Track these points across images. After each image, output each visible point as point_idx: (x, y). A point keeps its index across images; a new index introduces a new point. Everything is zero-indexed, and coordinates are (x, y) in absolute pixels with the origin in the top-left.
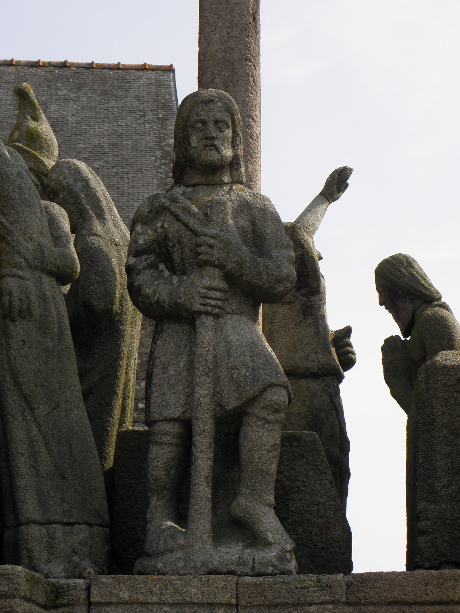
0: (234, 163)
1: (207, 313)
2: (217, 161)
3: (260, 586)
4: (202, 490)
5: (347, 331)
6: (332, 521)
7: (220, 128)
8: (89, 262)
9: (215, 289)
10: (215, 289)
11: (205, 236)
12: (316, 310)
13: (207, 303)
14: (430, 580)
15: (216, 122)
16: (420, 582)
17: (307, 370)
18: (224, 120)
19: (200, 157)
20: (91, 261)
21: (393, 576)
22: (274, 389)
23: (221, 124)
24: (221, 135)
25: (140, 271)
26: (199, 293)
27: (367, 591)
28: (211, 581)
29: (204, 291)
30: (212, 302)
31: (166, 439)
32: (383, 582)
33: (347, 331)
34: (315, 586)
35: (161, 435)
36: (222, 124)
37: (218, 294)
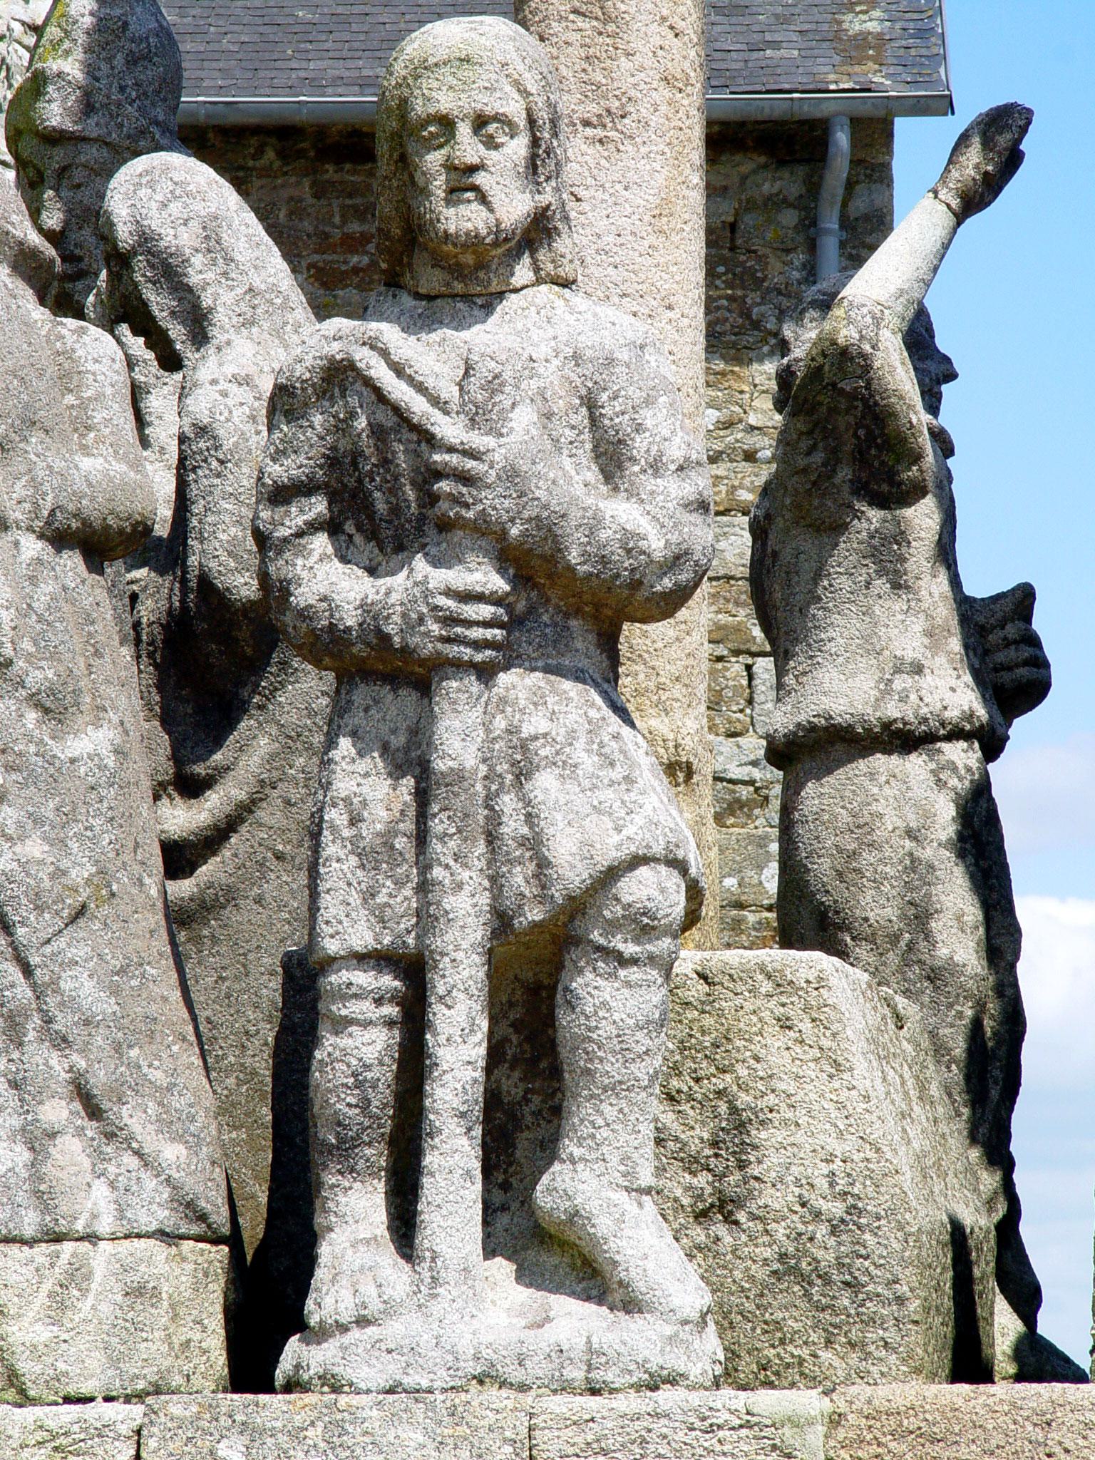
0: (538, 231)
1: (460, 666)
2: (484, 232)
3: (591, 1424)
4: (454, 1161)
5: (1023, 598)
6: (869, 1208)
7: (491, 137)
8: (215, 464)
9: (479, 598)
10: (479, 598)
11: (451, 449)
12: (914, 544)
13: (457, 635)
14: (1059, 1414)
15: (480, 122)
16: (1027, 1418)
17: (887, 725)
18: (503, 114)
19: (438, 221)
20: (218, 460)
21: (955, 1400)
22: (643, 872)
23: (491, 128)
24: (493, 154)
25: (285, 540)
26: (436, 608)
27: (884, 1440)
28: (460, 1409)
29: (451, 603)
30: (476, 633)
31: (364, 1009)
32: (928, 1416)
33: (1023, 598)
34: (741, 1426)
35: (344, 998)
36: (495, 125)
37: (486, 611)
